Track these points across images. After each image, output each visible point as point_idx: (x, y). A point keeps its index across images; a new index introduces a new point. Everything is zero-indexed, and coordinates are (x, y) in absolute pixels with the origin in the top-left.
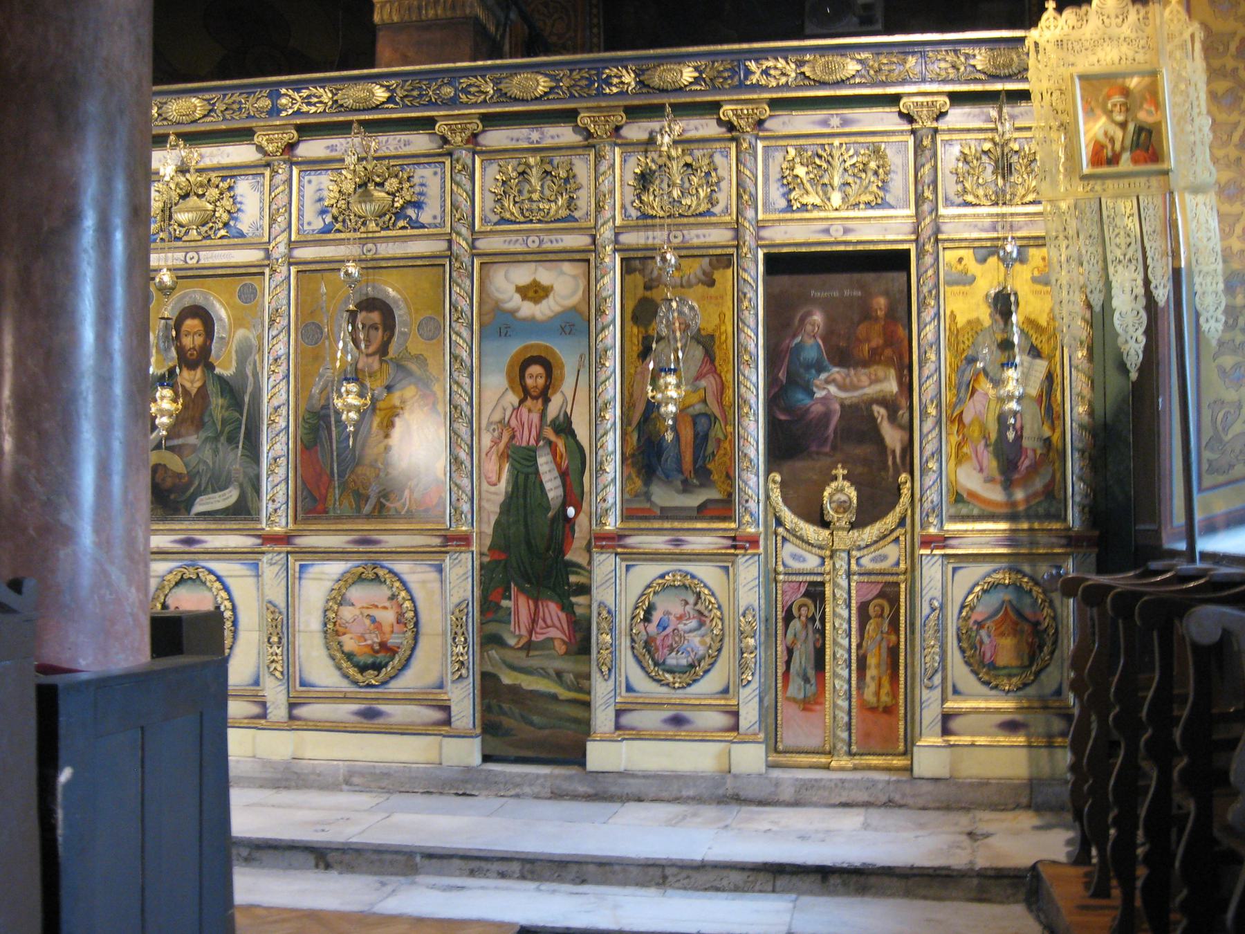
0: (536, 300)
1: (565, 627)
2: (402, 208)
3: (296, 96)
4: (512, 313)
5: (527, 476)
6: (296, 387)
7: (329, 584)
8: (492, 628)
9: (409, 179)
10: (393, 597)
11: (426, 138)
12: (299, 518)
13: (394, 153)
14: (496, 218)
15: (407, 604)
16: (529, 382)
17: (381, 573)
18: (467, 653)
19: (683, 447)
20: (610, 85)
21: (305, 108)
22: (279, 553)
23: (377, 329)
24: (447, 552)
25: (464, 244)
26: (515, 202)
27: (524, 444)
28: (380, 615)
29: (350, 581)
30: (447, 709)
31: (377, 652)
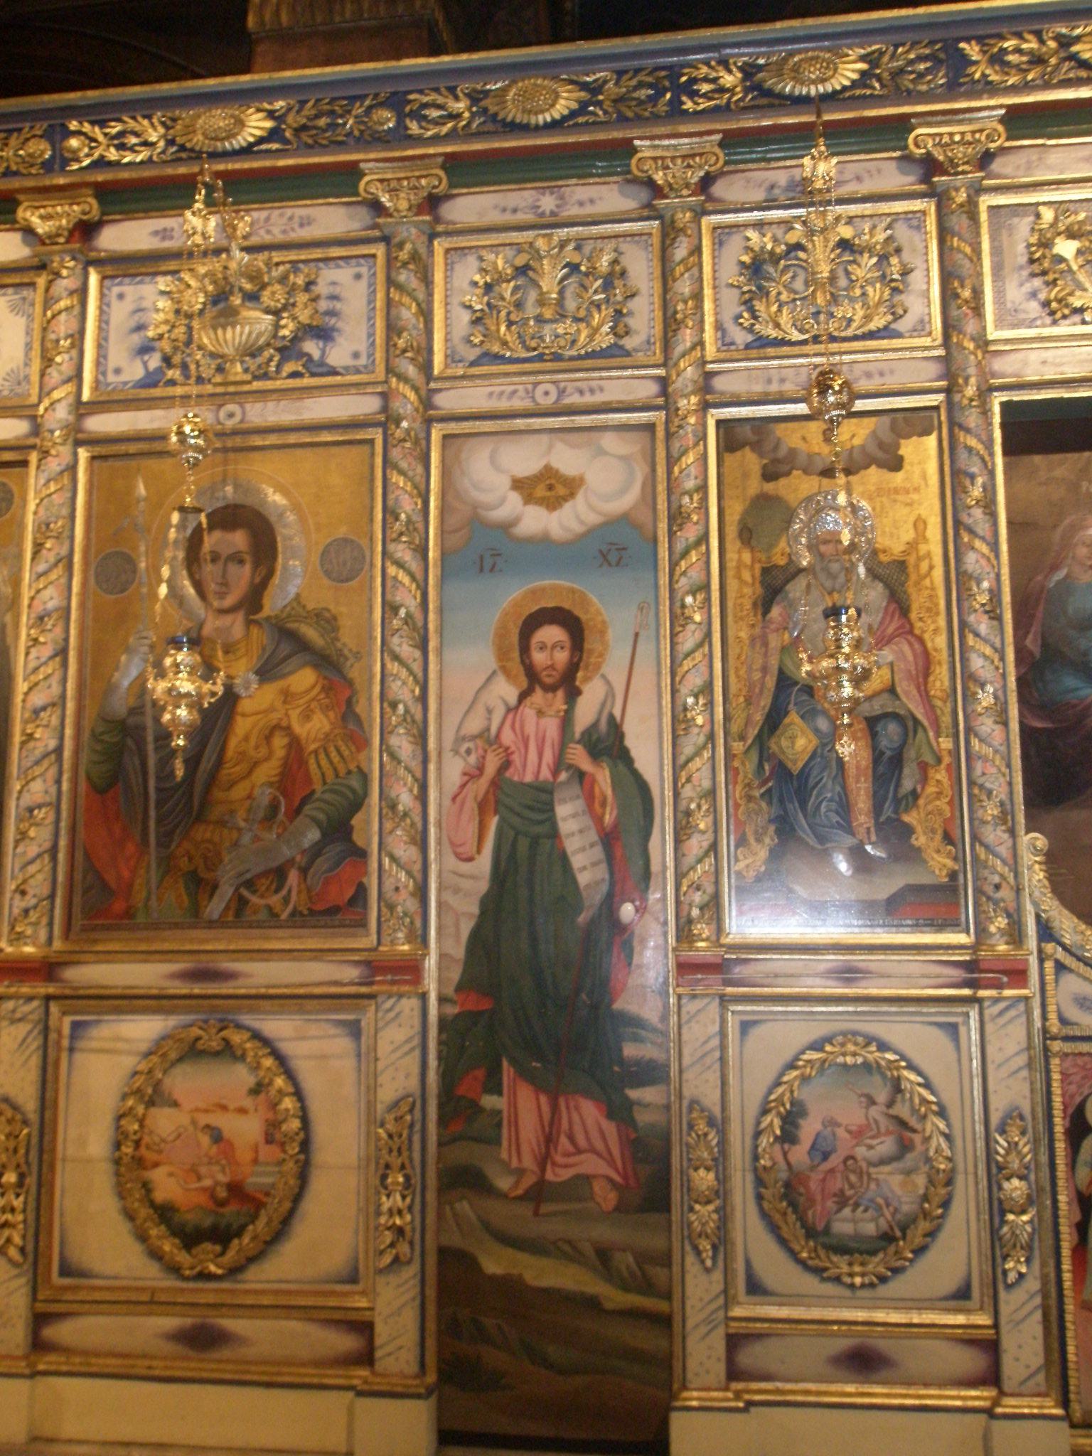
0: (553, 504)
1: (616, 1152)
2: (296, 339)
3: (97, 132)
4: (505, 528)
5: (535, 841)
6: (80, 671)
7: (129, 1062)
8: (462, 1154)
9: (309, 285)
10: (257, 1090)
11: (342, 211)
12: (78, 923)
13: (279, 237)
14: (473, 354)
15: (288, 1103)
16: (539, 658)
17: (237, 1038)
18: (410, 1208)
19: (851, 781)
20: (693, 94)
21: (113, 155)
22: (30, 999)
23: (241, 562)
24: (371, 996)
25: (412, 396)
26: (510, 323)
27: (529, 778)
28: (229, 1124)
29: (173, 1055)
30: (364, 1328)
31: (222, 1203)
